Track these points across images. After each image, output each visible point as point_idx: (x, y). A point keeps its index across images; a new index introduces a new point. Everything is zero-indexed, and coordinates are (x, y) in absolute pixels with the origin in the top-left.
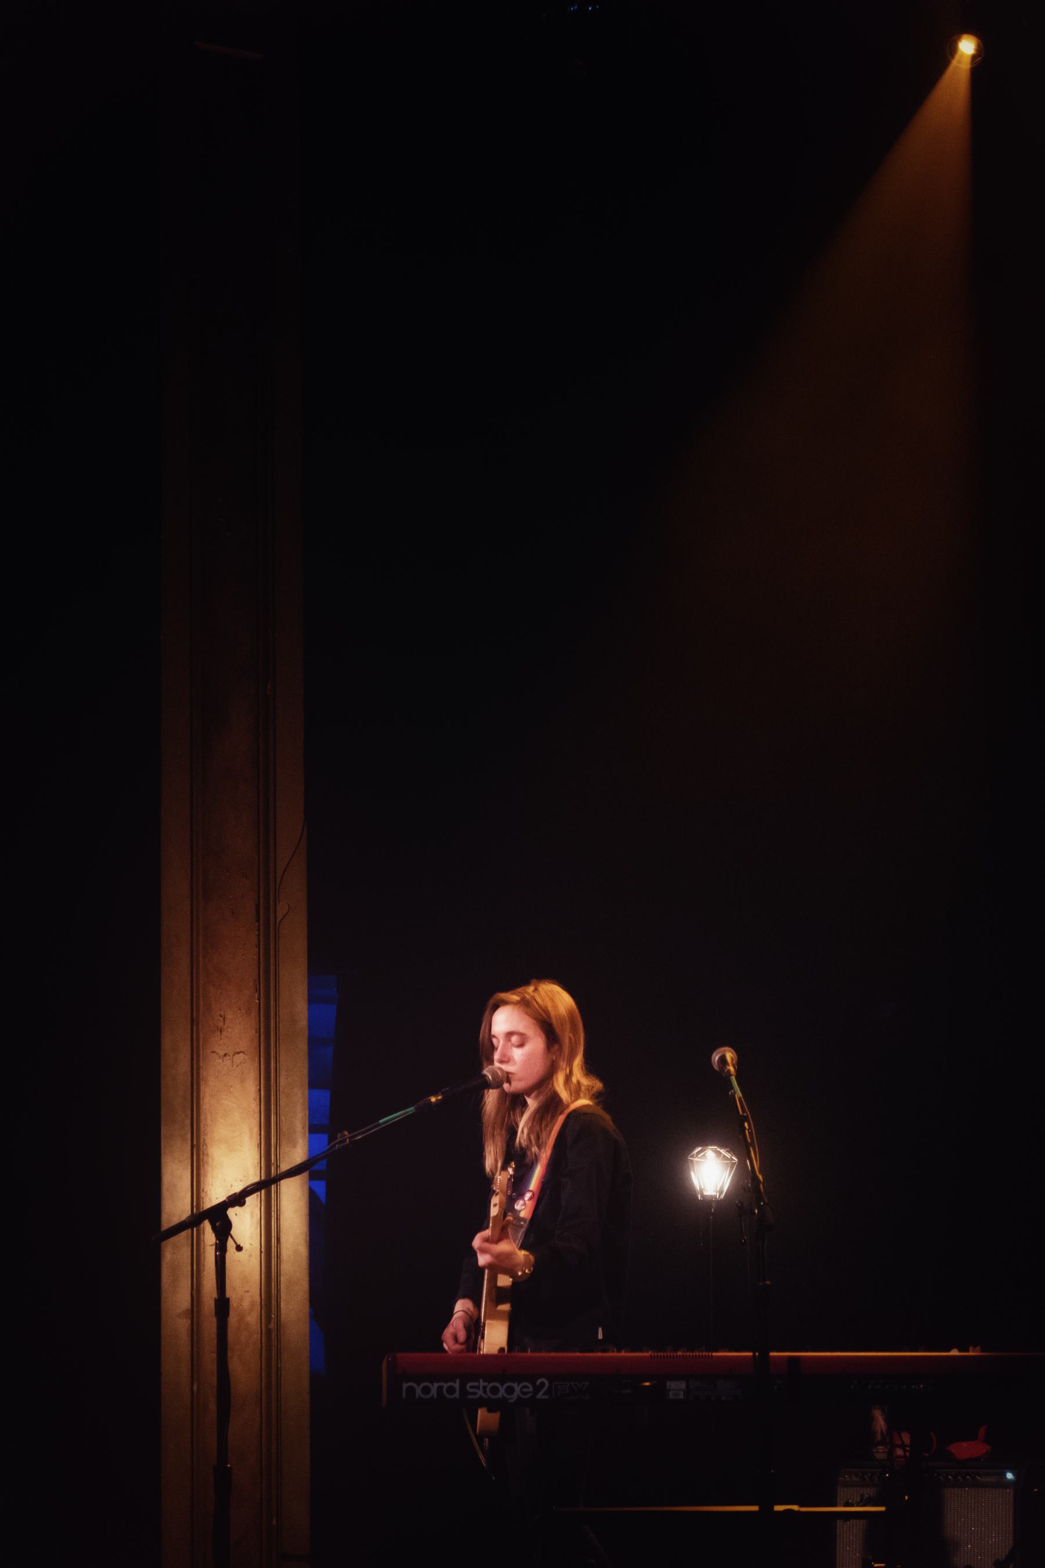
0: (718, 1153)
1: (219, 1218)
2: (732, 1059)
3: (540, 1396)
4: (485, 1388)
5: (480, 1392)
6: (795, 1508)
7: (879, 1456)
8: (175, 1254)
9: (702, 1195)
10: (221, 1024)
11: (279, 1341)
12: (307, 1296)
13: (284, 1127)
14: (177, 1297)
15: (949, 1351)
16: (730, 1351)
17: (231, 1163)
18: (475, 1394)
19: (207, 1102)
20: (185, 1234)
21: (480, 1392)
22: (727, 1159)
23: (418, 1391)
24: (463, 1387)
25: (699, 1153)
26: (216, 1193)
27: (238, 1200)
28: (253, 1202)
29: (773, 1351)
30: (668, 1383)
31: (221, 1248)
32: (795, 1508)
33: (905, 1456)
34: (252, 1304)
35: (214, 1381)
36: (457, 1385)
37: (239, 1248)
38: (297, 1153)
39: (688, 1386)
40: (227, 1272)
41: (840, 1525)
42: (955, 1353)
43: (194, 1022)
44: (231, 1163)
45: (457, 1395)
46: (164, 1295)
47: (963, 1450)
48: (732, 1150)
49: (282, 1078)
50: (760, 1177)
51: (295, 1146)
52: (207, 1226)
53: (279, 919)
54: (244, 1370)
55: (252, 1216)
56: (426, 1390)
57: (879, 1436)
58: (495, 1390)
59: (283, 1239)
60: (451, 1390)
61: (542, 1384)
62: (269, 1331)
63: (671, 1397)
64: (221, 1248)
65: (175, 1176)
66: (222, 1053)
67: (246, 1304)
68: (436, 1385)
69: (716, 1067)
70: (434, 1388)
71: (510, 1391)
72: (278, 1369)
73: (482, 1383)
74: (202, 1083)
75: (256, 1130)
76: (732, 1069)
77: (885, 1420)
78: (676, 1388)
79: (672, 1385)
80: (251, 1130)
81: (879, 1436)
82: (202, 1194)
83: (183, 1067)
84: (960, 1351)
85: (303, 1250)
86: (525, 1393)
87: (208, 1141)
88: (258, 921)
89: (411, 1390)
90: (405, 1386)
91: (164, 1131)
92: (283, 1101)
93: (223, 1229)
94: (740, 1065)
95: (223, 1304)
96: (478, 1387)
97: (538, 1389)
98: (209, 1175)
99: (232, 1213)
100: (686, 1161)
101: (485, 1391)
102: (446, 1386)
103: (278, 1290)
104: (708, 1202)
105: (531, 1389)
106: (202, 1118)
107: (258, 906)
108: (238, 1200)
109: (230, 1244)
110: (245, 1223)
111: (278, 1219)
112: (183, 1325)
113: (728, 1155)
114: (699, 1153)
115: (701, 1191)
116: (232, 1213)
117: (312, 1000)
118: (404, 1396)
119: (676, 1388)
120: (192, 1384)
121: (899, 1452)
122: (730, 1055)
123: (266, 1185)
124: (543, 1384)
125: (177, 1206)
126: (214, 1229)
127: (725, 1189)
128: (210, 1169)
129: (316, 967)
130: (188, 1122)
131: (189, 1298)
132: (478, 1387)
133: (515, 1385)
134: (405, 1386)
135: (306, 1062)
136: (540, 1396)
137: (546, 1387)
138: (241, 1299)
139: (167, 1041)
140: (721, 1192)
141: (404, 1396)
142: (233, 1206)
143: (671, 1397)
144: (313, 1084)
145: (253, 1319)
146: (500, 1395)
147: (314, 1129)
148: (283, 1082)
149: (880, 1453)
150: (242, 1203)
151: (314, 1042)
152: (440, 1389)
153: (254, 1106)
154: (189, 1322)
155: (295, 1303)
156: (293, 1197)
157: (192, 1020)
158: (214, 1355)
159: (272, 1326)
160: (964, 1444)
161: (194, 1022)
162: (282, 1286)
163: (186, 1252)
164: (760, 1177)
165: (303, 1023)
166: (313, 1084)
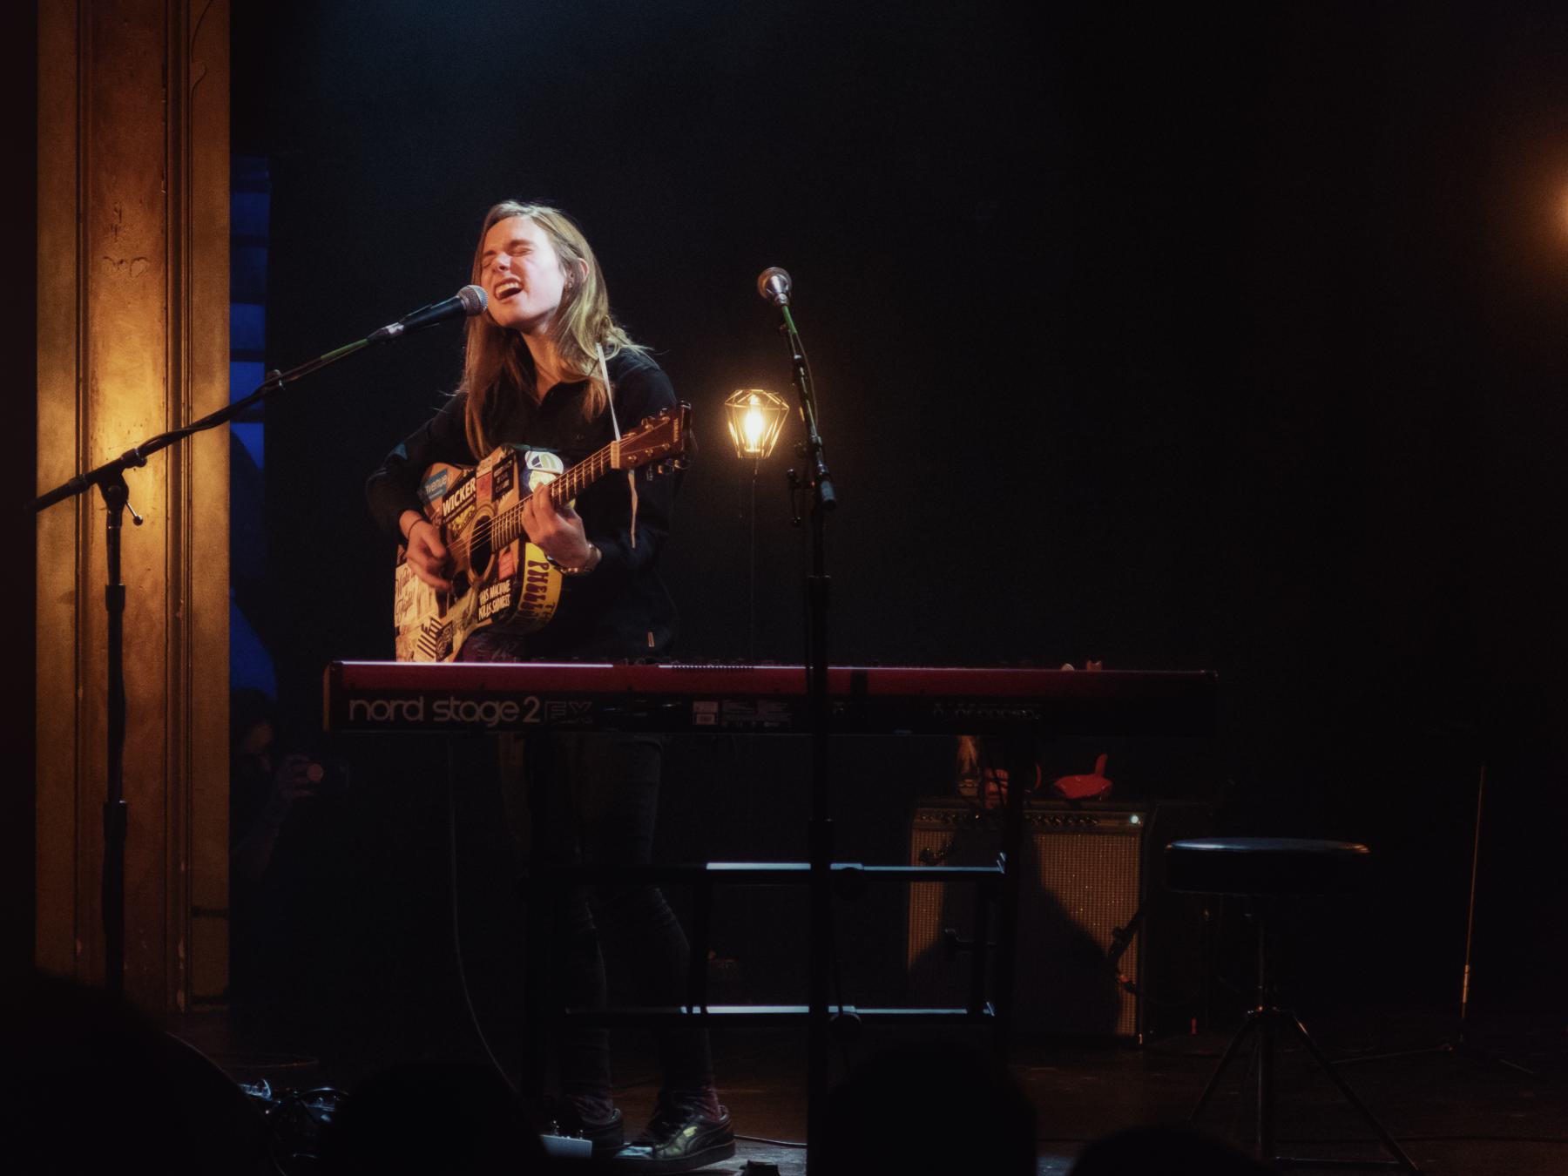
0: (763, 398)
1: (112, 481)
2: (784, 284)
3: (528, 719)
4: (457, 707)
5: (451, 713)
6: (859, 866)
7: (965, 792)
8: (54, 525)
9: (743, 453)
10: (116, 222)
11: (190, 633)
12: (227, 577)
13: (198, 359)
14: (56, 576)
16: (793, 663)
17: (129, 412)
18: (444, 715)
19: (97, 327)
20: (67, 504)
22: (773, 404)
23: (370, 709)
24: (428, 707)
25: (738, 398)
26: (109, 449)
27: (135, 458)
28: (157, 460)
29: (833, 664)
30: (696, 704)
31: (115, 521)
32: (859, 866)
33: (999, 793)
34: (155, 584)
35: (105, 685)
36: (421, 705)
37: (138, 521)
38: (213, 395)
39: (720, 706)
40: (122, 554)
41: (917, 888)
44: (129, 412)
45: (420, 716)
47: (1079, 785)
49: (197, 287)
51: (211, 382)
52: (96, 488)
53: (192, 85)
54: (144, 674)
55: (156, 472)
56: (381, 710)
57: (967, 768)
58: (470, 711)
59: (196, 502)
60: (413, 710)
61: (532, 704)
62: (176, 621)
63: (699, 722)
64: (115, 521)
65: (55, 415)
66: (117, 259)
67: (147, 585)
68: (394, 704)
71: (489, 711)
72: (189, 671)
73: (453, 702)
74: (91, 298)
75: (161, 360)
77: (975, 746)
78: (706, 712)
79: (699, 706)
80: (155, 364)
81: (967, 768)
82: (91, 443)
85: (223, 517)
86: (511, 716)
87: (99, 374)
88: (165, 86)
89: (361, 710)
90: (353, 704)
91: (42, 360)
92: (196, 323)
93: (118, 496)
94: (793, 294)
95: (116, 594)
97: (525, 710)
98: (99, 418)
99: (131, 476)
100: (721, 403)
101: (457, 713)
102: (406, 704)
103: (189, 568)
104: (751, 461)
105: (517, 710)
106: (91, 343)
107: (165, 68)
108: (135, 458)
109: (127, 518)
110: (147, 488)
111: (189, 476)
112: (65, 612)
113: (777, 402)
114: (738, 398)
115: (742, 446)
116: (131, 476)
117: (236, 187)
118: (352, 717)
119: (706, 712)
120: (77, 688)
121: (993, 787)
123: (173, 439)
124: (532, 704)
125: (56, 463)
126: (106, 496)
127: (773, 443)
128: (97, 408)
130: (73, 348)
132: (448, 707)
133: (496, 705)
134: (353, 704)
135: (227, 272)
136: (528, 719)
137: (534, 711)
138: (142, 579)
139: (45, 243)
140: (767, 448)
141: (352, 717)
142: (129, 466)
143: (699, 722)
144: (236, 298)
145: (156, 605)
146: (476, 718)
147: (238, 355)
148: (196, 300)
149: (968, 788)
150: (142, 464)
151: (239, 242)
152: (399, 708)
153: (159, 328)
154: (73, 608)
155: (211, 585)
156: (208, 456)
158: (105, 651)
159: (181, 614)
160: (1078, 779)
161: (80, 217)
162: (195, 564)
163: (70, 519)
165: (224, 220)
166: (237, 297)
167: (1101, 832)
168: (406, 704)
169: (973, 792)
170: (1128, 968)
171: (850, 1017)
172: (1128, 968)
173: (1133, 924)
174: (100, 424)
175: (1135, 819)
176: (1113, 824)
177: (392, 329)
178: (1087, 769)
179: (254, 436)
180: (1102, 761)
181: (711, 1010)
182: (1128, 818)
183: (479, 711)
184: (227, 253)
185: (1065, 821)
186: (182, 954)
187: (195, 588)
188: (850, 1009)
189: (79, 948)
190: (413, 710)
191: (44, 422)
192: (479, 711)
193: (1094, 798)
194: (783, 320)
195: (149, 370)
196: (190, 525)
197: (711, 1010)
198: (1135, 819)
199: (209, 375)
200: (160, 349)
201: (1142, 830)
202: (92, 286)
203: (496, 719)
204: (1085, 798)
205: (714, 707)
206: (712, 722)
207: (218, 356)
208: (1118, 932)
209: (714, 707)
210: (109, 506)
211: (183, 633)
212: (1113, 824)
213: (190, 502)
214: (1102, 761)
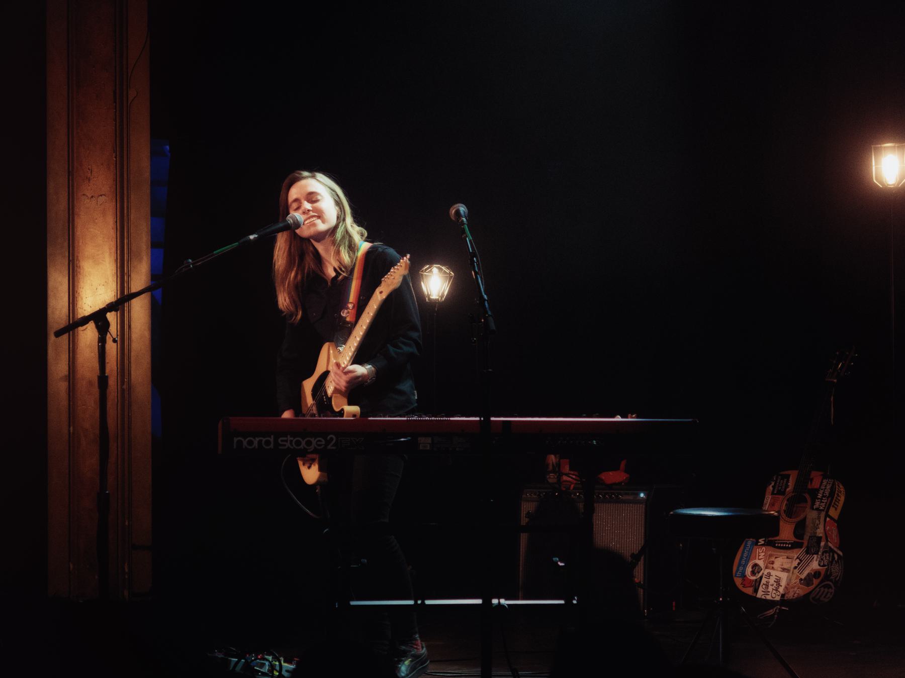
0: (440, 269)
3: (329, 447)
4: (291, 441)
5: (288, 444)
7: (550, 481)
9: (429, 299)
12: (149, 366)
14: (58, 367)
15: (614, 417)
16: (462, 416)
19: (79, 232)
21: (288, 444)
23: (245, 443)
36: (272, 439)
42: (618, 419)
43: (70, 173)
45: (272, 446)
46: (49, 364)
47: (612, 477)
48: (450, 267)
49: (133, 211)
50: (485, 297)
57: (551, 467)
58: (298, 443)
59: (133, 326)
60: (268, 443)
61: (332, 439)
62: (123, 390)
65: (57, 281)
68: (257, 439)
69: (453, 218)
70: (256, 442)
71: (309, 443)
73: (289, 438)
75: (114, 249)
76: (464, 219)
78: (425, 443)
79: (421, 440)
80: (110, 249)
81: (551, 467)
83: (63, 205)
84: (622, 417)
85: (147, 334)
88: (115, 102)
89: (240, 442)
90: (236, 440)
91: (50, 250)
94: (470, 217)
96: (286, 441)
97: (328, 442)
102: (264, 440)
103: (130, 362)
105: (323, 442)
107: (115, 93)
112: (63, 386)
113: (448, 271)
115: (429, 296)
119: (425, 443)
122: (463, 209)
124: (332, 439)
127: (446, 293)
129: (156, 135)
130: (66, 244)
131: (67, 368)
132: (286, 441)
133: (312, 440)
134: (236, 440)
136: (329, 447)
139: (51, 187)
140: (442, 297)
146: (301, 447)
149: (552, 478)
152: (260, 442)
153: (112, 233)
157: (69, 172)
159: (125, 387)
161: (70, 173)
162: (133, 359)
164: (485, 297)
165: (147, 174)
167: (624, 502)
168: (264, 440)
169: (555, 480)
170: (639, 574)
171: (503, 606)
172: (639, 574)
173: (642, 551)
174: (81, 284)
175: (642, 495)
176: (631, 498)
177: (252, 237)
178: (616, 468)
179: (158, 292)
180: (623, 464)
181: (428, 602)
182: (638, 495)
183: (303, 443)
184: (148, 191)
185: (604, 496)
186: (127, 570)
187: (132, 373)
188: (503, 601)
189: (71, 566)
190: (268, 443)
191: (51, 284)
192: (303, 443)
193: (620, 484)
194: (464, 231)
195: (107, 255)
196: (130, 338)
197: (428, 602)
198: (642, 495)
199: (140, 260)
200: (113, 243)
201: (645, 501)
202: (76, 210)
203: (312, 448)
204: (615, 484)
205: (429, 440)
206: (428, 448)
207: (145, 247)
208: (633, 555)
209: (429, 440)
210: (324, 387)
211: (126, 396)
212: (631, 498)
213: (130, 327)
214: (623, 464)
